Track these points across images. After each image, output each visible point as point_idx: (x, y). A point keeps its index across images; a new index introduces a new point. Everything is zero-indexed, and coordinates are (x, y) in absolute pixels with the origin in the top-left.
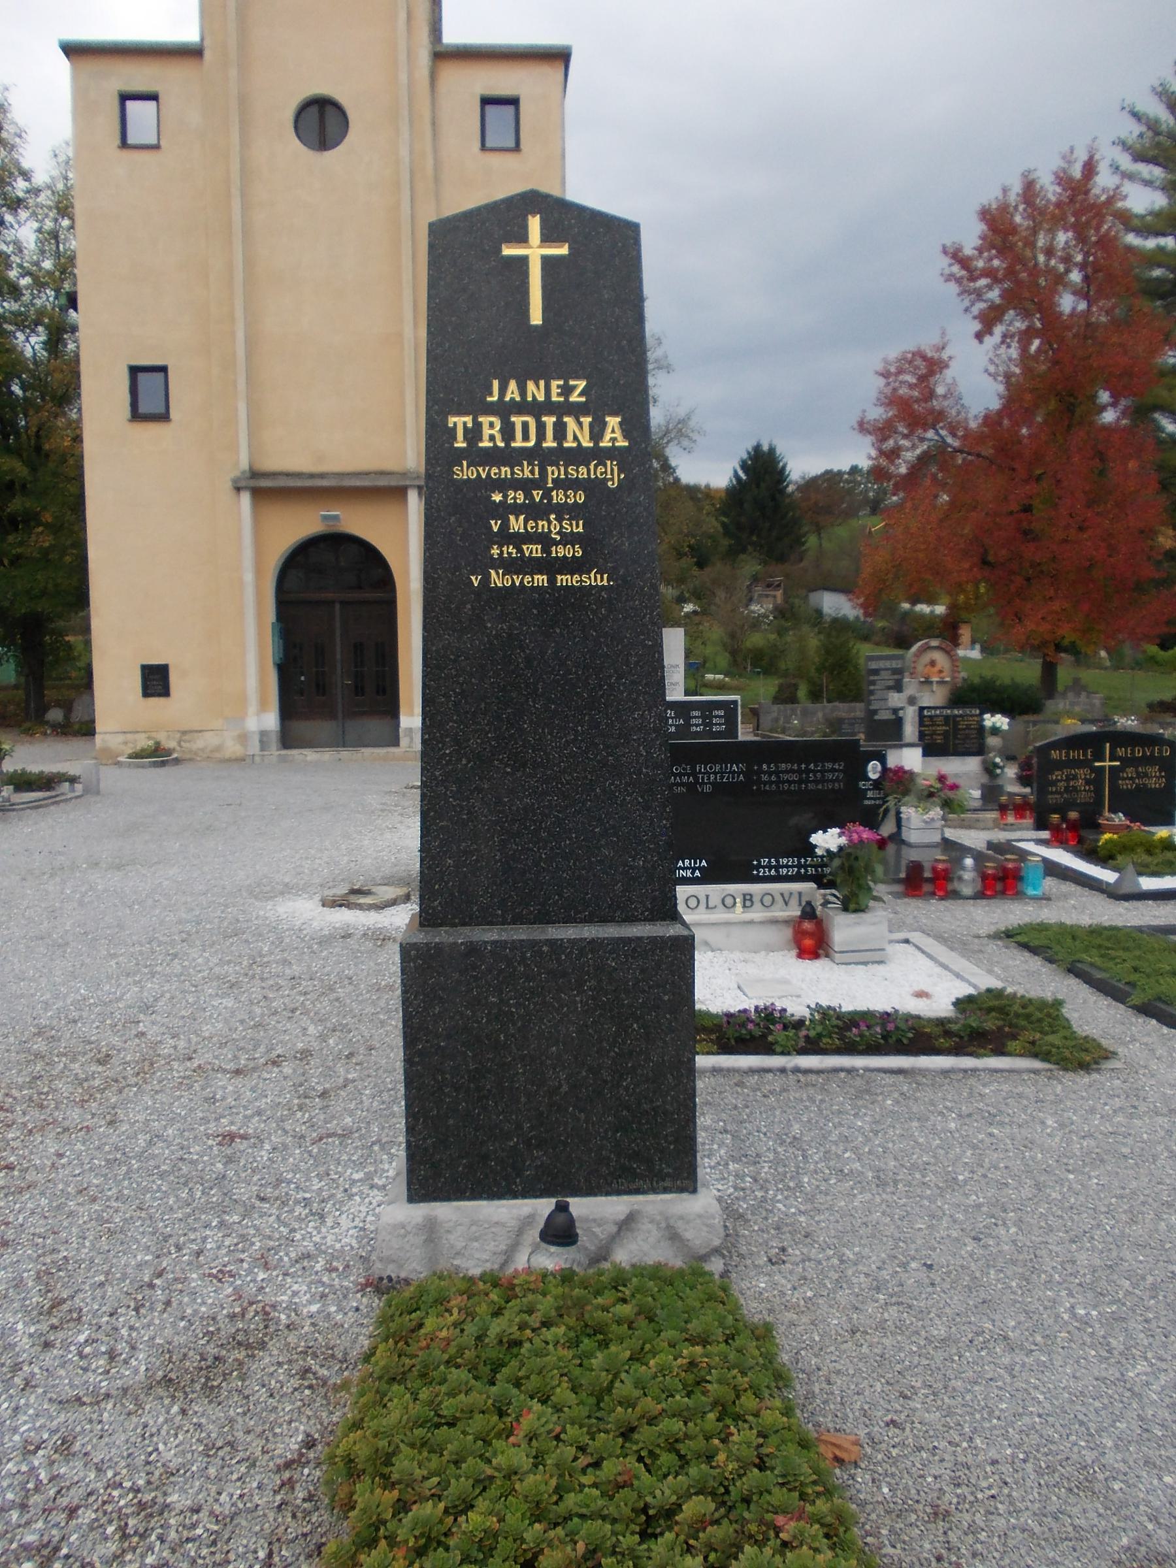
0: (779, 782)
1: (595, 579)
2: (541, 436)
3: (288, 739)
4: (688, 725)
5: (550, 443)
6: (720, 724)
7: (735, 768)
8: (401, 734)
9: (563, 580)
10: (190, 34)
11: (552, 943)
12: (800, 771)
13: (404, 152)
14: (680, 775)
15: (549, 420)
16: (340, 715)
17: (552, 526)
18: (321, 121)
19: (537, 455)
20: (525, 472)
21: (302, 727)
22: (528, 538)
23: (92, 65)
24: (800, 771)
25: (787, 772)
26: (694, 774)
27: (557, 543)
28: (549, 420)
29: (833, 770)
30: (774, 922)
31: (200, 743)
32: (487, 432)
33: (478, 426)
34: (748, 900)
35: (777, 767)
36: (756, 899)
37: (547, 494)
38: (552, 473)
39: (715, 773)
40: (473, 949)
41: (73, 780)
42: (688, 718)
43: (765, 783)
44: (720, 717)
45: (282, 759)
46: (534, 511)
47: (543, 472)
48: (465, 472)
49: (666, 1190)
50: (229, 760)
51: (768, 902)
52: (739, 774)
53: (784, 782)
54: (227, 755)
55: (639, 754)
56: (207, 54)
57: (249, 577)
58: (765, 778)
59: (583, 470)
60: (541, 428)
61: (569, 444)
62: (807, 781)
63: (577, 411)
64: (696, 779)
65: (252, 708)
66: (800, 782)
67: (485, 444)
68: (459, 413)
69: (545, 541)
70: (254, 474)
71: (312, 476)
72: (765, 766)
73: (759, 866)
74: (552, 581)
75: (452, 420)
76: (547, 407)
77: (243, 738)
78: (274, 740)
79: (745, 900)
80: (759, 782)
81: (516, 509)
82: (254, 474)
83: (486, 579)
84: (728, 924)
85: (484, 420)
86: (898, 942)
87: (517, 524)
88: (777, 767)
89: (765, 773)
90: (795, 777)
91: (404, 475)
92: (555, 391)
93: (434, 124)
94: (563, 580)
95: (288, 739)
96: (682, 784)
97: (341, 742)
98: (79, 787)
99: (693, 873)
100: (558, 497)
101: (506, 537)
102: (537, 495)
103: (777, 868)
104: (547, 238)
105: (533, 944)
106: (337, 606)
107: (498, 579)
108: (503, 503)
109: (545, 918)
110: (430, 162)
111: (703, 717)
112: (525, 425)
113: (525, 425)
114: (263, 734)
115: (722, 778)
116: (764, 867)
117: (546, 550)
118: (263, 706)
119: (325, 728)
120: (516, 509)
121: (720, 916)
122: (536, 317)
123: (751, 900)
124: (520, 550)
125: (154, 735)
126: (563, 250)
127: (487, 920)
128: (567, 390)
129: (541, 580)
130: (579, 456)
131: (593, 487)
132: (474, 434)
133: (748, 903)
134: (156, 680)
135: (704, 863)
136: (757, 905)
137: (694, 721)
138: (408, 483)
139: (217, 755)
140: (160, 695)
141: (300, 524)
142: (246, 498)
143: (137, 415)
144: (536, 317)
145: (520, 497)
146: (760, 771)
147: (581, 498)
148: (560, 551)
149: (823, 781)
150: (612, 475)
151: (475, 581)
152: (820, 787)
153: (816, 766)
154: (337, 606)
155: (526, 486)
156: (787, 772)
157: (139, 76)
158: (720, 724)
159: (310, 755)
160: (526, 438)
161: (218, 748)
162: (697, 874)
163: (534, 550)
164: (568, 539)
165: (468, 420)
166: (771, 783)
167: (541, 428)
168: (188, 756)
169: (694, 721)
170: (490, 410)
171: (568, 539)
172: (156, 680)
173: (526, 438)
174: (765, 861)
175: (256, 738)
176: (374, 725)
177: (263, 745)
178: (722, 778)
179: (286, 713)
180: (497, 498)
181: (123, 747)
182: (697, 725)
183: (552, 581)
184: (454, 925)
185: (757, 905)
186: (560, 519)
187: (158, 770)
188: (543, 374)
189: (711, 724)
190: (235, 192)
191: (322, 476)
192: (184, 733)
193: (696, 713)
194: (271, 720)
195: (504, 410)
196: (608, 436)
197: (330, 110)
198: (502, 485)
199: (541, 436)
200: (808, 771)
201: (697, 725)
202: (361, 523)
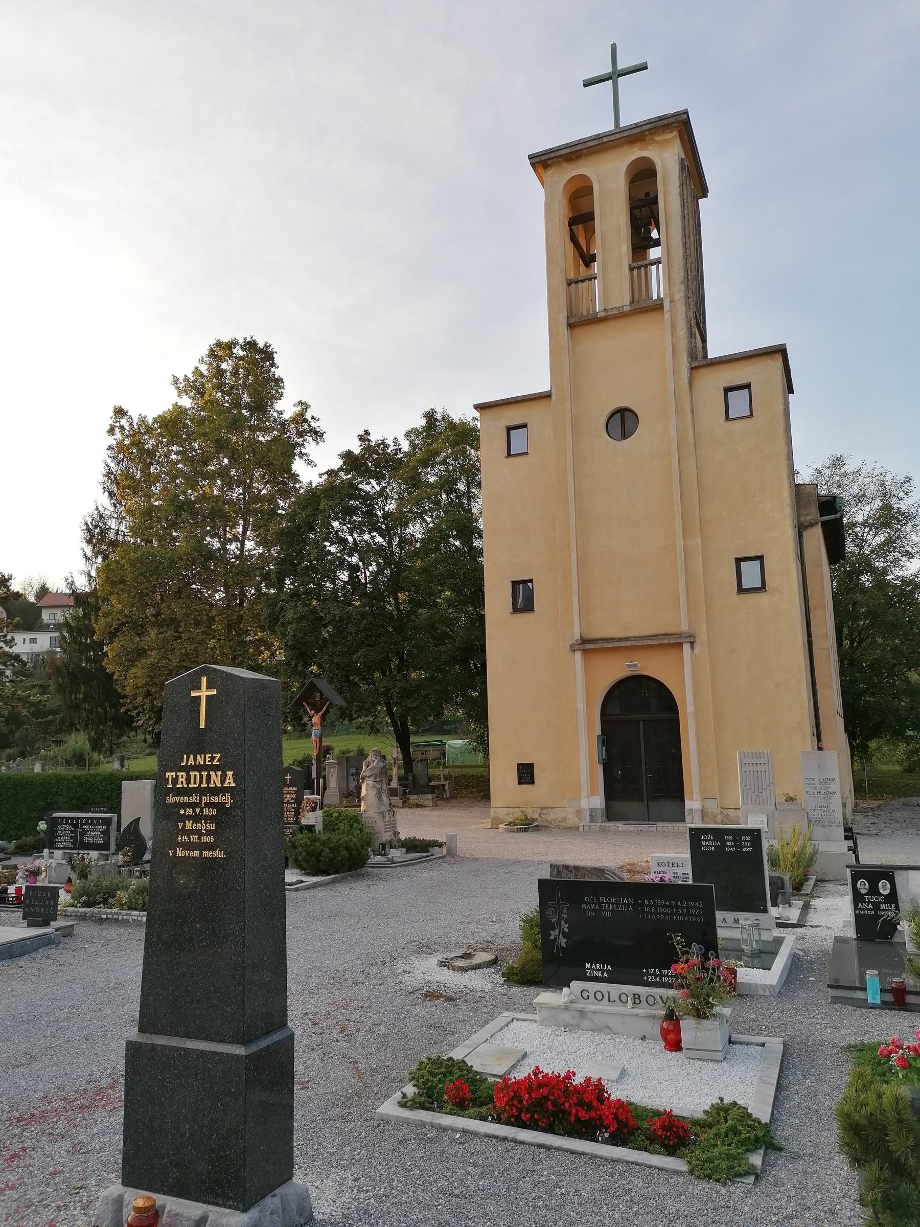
0: (657, 913)
1: (218, 854)
2: (201, 782)
3: (611, 815)
4: (723, 846)
5: (204, 785)
6: (748, 847)
7: (625, 900)
8: (686, 814)
9: (206, 854)
10: (544, 386)
11: (186, 1049)
12: (671, 906)
13: (673, 432)
14: (590, 903)
15: (205, 774)
16: (645, 799)
17: (202, 826)
18: (623, 422)
19: (200, 791)
20: (194, 799)
21: (618, 806)
22: (193, 832)
23: (490, 413)
24: (671, 906)
25: (662, 906)
26: (599, 904)
27: (204, 835)
28: (205, 774)
29: (695, 907)
30: (652, 1017)
31: (552, 816)
32: (180, 780)
33: (177, 776)
34: (636, 999)
35: (655, 903)
36: (643, 999)
37: (201, 811)
38: (205, 799)
39: (613, 904)
40: (154, 1047)
41: (440, 845)
42: (723, 842)
43: (647, 913)
44: (747, 841)
45: (603, 830)
46: (196, 819)
47: (201, 799)
48: (171, 800)
49: (230, 1207)
50: (570, 828)
51: (651, 1002)
52: (629, 905)
53: (660, 914)
54: (569, 825)
55: (231, 949)
56: (553, 396)
57: (581, 706)
58: (647, 910)
59: (216, 798)
60: (201, 777)
61: (212, 785)
62: (677, 914)
63: (216, 768)
64: (600, 906)
65: (584, 794)
66: (672, 914)
67: (180, 786)
68: (170, 771)
69: (199, 833)
70: (584, 641)
71: (620, 640)
72: (646, 901)
73: (647, 974)
74: (201, 854)
75: (168, 774)
76: (204, 767)
77: (579, 813)
78: (600, 816)
79: (635, 998)
80: (643, 912)
81: (189, 818)
82: (584, 641)
83: (175, 853)
84: (620, 1014)
85: (180, 774)
86: (757, 1045)
87: (189, 825)
88: (655, 903)
89: (647, 906)
90: (668, 910)
91: (680, 635)
92: (208, 759)
93: (692, 411)
94: (206, 854)
95: (611, 815)
96: (592, 910)
97: (648, 818)
98: (444, 849)
99: (602, 974)
100: (206, 812)
101: (185, 832)
102: (198, 810)
103: (661, 976)
104: (209, 687)
105: (178, 1048)
106: (641, 723)
107: (180, 853)
108: (184, 814)
109: (187, 1035)
110: (691, 434)
111: (734, 840)
112: (195, 775)
113: (195, 775)
114: (592, 810)
115: (618, 907)
116: (651, 975)
117: (200, 838)
118: (593, 792)
119: (636, 807)
120: (189, 818)
121: (617, 1008)
122: (202, 725)
123: (639, 998)
124: (189, 838)
125: (524, 809)
126: (214, 692)
127: (162, 1032)
128: (212, 759)
129: (196, 853)
130: (215, 791)
131: (220, 806)
132: (175, 781)
133: (637, 1001)
134: (526, 774)
135: (609, 967)
136: (644, 1003)
137: (728, 843)
138: (682, 640)
139: (563, 824)
140: (528, 783)
141: (614, 670)
142: (578, 655)
143: (516, 610)
144: (202, 725)
145: (190, 811)
146: (643, 904)
147: (214, 812)
148: (205, 839)
149: (688, 914)
150: (227, 800)
151: (171, 852)
152: (686, 919)
153: (682, 904)
154: (641, 723)
155: (193, 806)
156: (662, 906)
157: (514, 416)
158: (748, 847)
159: (621, 826)
160: (195, 783)
161: (564, 820)
162: (605, 974)
163: (194, 838)
164: (209, 833)
165: (174, 774)
166: (652, 914)
167: (201, 777)
168: (545, 824)
169: (728, 843)
170: (182, 769)
171: (209, 833)
172: (526, 774)
173: (195, 783)
174: (651, 970)
175: (587, 814)
176: (669, 806)
177: (592, 818)
178: (618, 907)
179: (610, 795)
180: (182, 812)
181: (506, 817)
182: (731, 847)
183: (201, 854)
184: (151, 1033)
185: (644, 1003)
186: (206, 823)
187: (523, 834)
188: (202, 751)
189: (741, 847)
190: (570, 473)
191: (627, 639)
192: (543, 808)
193: (730, 838)
194: (598, 801)
195: (187, 769)
196: (227, 781)
197: (627, 414)
198: (184, 806)
199: (201, 782)
200: (677, 907)
201: (731, 847)
202: (653, 666)
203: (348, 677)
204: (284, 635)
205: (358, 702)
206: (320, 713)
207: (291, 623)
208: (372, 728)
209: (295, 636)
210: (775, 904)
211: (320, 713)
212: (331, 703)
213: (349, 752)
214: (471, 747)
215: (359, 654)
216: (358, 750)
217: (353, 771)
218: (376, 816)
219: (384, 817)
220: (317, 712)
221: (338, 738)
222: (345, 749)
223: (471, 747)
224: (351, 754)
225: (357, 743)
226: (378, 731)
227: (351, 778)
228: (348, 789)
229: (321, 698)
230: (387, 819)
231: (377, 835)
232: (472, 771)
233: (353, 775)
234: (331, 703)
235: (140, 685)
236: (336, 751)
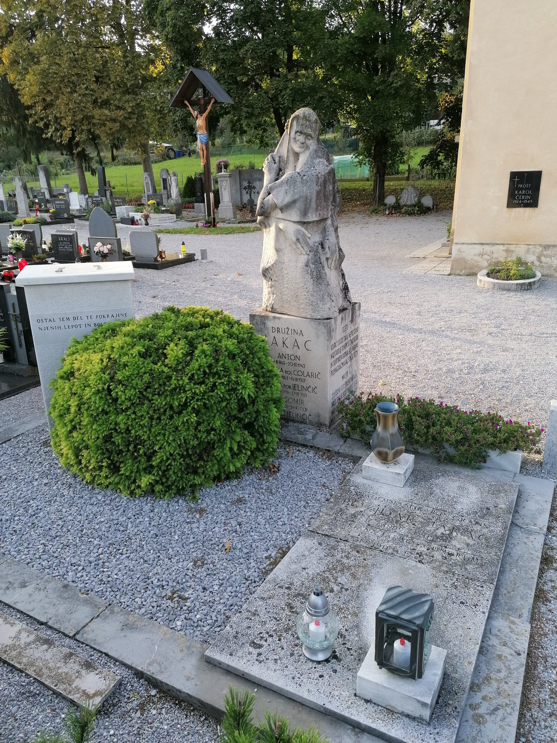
134: (524, 188)
140: (526, 205)
192: (547, 247)
203: (236, 78)
204: (164, 25)
205: (247, 107)
206: (205, 115)
207: (168, 9)
208: (261, 142)
209: (174, 26)
210: (534, 276)
211: (205, 115)
212: (216, 102)
213: (242, 167)
214: (357, 160)
215: (246, 48)
216: (250, 166)
217: (246, 184)
218: (310, 331)
219: (330, 332)
220: (201, 113)
221: (234, 157)
222: (238, 164)
223: (357, 160)
224: (244, 168)
225: (249, 160)
226: (267, 144)
227: (244, 192)
228: (242, 202)
229: (205, 96)
230: (338, 335)
231: (310, 382)
232: (353, 185)
233: (245, 188)
234: (216, 102)
235: (34, 93)
236: (231, 167)
